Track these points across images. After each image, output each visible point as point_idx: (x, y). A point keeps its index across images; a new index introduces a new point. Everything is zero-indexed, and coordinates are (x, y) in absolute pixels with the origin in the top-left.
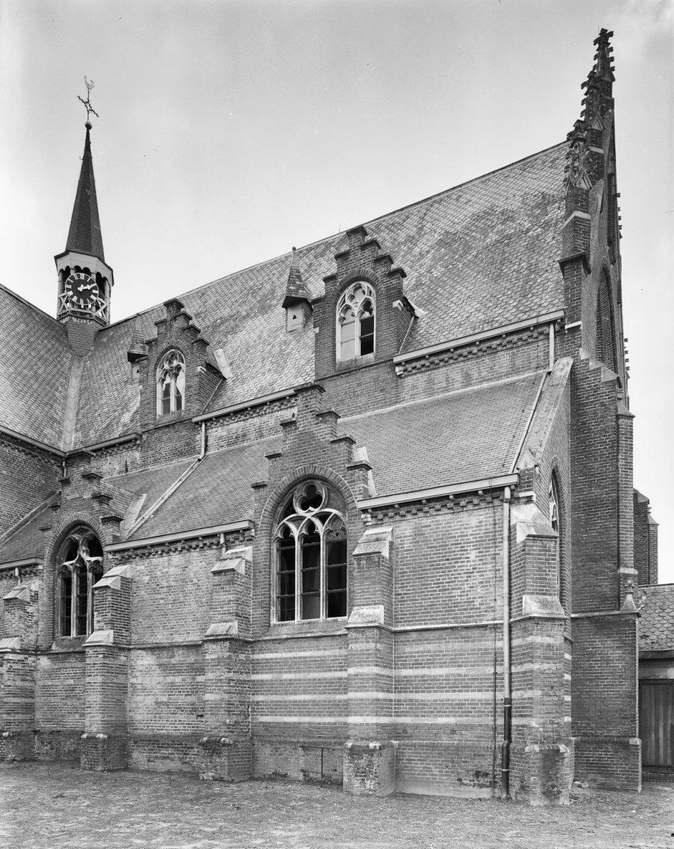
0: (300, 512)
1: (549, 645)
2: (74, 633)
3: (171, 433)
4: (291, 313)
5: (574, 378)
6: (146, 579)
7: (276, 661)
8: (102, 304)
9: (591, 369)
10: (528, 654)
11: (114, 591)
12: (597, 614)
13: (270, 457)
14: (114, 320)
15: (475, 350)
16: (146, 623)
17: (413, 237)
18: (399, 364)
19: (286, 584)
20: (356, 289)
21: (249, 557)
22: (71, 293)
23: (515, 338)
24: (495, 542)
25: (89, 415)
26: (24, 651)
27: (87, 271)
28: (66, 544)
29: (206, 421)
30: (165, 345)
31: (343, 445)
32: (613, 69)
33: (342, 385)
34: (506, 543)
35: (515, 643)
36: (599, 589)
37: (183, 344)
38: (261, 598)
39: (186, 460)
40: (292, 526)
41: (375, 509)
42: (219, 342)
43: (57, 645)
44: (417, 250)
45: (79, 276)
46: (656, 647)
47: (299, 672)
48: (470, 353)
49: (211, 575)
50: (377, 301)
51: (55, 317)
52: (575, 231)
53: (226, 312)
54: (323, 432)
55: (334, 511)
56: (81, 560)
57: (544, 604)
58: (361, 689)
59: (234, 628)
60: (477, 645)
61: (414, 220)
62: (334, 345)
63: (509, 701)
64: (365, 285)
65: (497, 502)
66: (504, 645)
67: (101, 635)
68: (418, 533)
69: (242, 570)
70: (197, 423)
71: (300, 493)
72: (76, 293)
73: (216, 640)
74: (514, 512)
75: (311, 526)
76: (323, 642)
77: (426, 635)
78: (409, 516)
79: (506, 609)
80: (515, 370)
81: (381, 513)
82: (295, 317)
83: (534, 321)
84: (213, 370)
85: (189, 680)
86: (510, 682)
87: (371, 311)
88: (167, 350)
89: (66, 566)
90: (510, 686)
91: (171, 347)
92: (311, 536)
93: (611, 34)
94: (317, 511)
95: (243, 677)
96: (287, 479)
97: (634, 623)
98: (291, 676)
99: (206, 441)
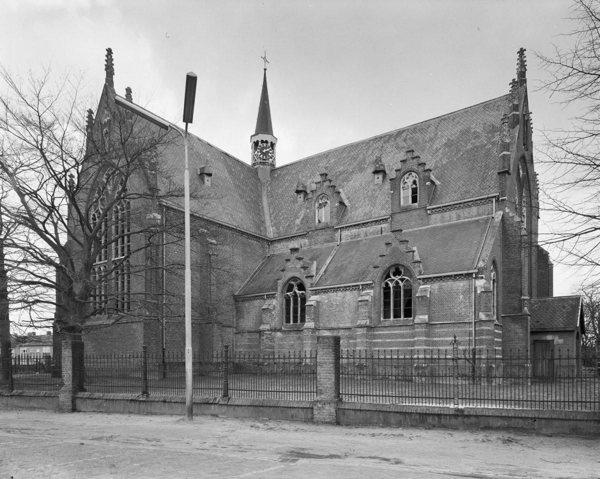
0: (393, 277)
1: (489, 330)
2: (299, 321)
3: (323, 232)
4: (376, 176)
5: (503, 219)
6: (326, 301)
7: (384, 335)
8: (273, 156)
9: (510, 216)
10: (481, 333)
11: (315, 307)
12: (512, 315)
13: (380, 256)
14: (278, 165)
15: (462, 206)
16: (327, 319)
17: (432, 139)
18: (429, 210)
19: (387, 304)
20: (409, 175)
21: (372, 295)
22: (260, 154)
23: (479, 202)
24: (469, 291)
25: (277, 218)
26: (271, 330)
27: (266, 142)
28: (287, 285)
29: (340, 228)
30: (320, 193)
31: (411, 253)
32: (526, 65)
33: (403, 216)
34: (473, 293)
35: (477, 329)
36: (513, 305)
37: (329, 192)
38: (376, 310)
39: (331, 244)
40: (389, 283)
41: (424, 279)
42: (340, 185)
43: (284, 327)
44: (435, 147)
45: (263, 145)
46: (542, 327)
47: (393, 339)
48: (460, 206)
49: (285, 261)
50: (419, 182)
51: (249, 162)
52: (504, 160)
53: (341, 168)
54: (402, 248)
55: (407, 278)
56: (295, 292)
57: (487, 316)
58: (419, 345)
59: (367, 322)
60: (463, 329)
61: (432, 129)
62: (400, 199)
63: (475, 349)
64: (414, 174)
65: (470, 278)
66: (473, 329)
67: (309, 324)
68: (440, 288)
69: (370, 300)
70: (336, 229)
71: (393, 270)
72: (262, 153)
73: (361, 327)
74: (477, 282)
75: (397, 283)
76: (404, 328)
77: (444, 325)
78: (437, 282)
79: (473, 316)
80: (479, 215)
81: (426, 280)
82: (378, 178)
83: (487, 196)
84: (342, 203)
85: (346, 342)
86: (475, 343)
87: (416, 185)
88: (321, 195)
89: (287, 295)
90: (475, 344)
91: (323, 194)
92: (397, 287)
93: (525, 50)
94: (400, 277)
95: (371, 341)
96: (387, 265)
97: (527, 319)
98: (390, 340)
99: (341, 236)
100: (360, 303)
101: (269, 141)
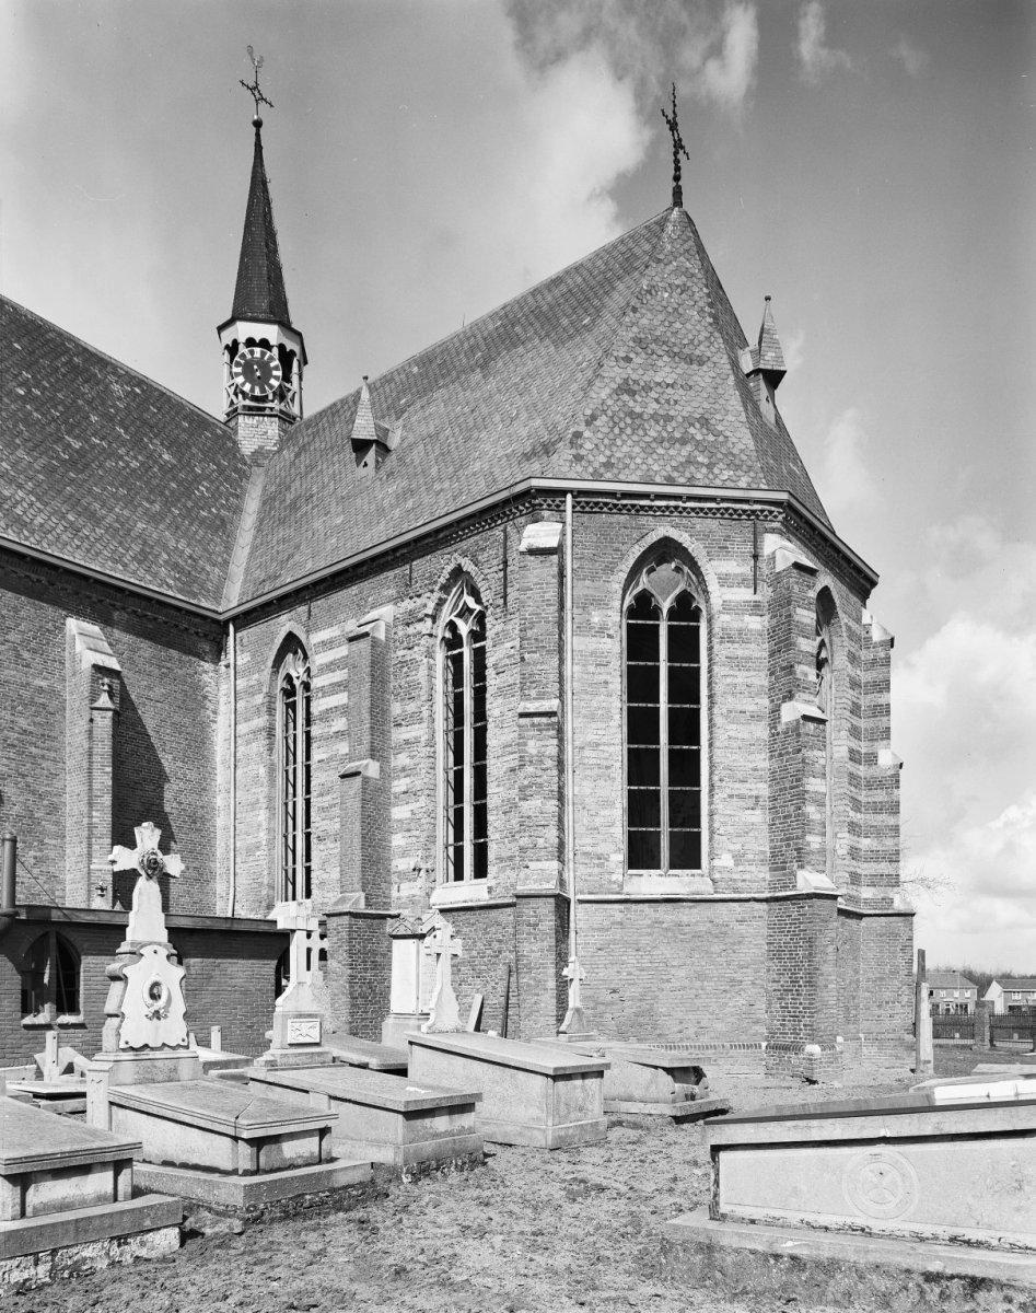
27: (264, 344)
45: (252, 353)
100: (524, 721)
101: (273, 342)
